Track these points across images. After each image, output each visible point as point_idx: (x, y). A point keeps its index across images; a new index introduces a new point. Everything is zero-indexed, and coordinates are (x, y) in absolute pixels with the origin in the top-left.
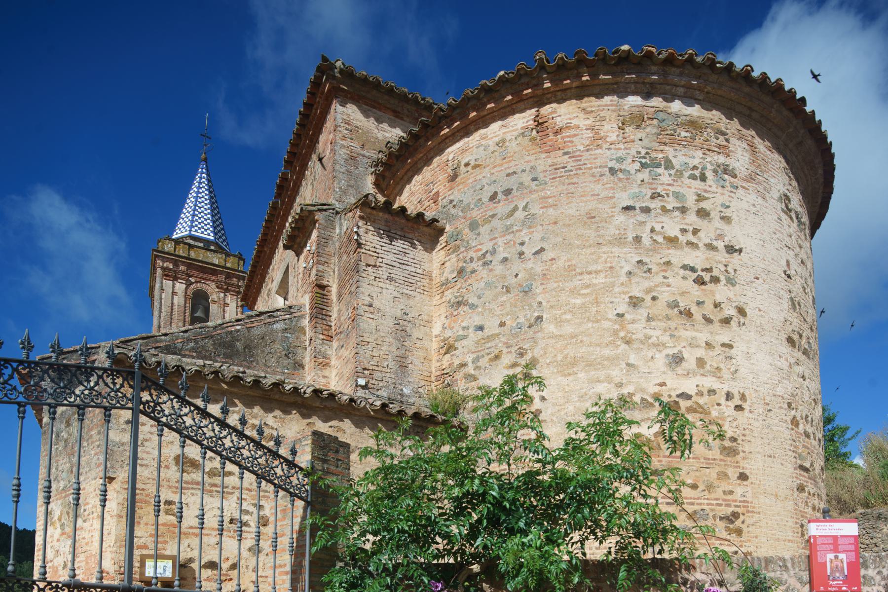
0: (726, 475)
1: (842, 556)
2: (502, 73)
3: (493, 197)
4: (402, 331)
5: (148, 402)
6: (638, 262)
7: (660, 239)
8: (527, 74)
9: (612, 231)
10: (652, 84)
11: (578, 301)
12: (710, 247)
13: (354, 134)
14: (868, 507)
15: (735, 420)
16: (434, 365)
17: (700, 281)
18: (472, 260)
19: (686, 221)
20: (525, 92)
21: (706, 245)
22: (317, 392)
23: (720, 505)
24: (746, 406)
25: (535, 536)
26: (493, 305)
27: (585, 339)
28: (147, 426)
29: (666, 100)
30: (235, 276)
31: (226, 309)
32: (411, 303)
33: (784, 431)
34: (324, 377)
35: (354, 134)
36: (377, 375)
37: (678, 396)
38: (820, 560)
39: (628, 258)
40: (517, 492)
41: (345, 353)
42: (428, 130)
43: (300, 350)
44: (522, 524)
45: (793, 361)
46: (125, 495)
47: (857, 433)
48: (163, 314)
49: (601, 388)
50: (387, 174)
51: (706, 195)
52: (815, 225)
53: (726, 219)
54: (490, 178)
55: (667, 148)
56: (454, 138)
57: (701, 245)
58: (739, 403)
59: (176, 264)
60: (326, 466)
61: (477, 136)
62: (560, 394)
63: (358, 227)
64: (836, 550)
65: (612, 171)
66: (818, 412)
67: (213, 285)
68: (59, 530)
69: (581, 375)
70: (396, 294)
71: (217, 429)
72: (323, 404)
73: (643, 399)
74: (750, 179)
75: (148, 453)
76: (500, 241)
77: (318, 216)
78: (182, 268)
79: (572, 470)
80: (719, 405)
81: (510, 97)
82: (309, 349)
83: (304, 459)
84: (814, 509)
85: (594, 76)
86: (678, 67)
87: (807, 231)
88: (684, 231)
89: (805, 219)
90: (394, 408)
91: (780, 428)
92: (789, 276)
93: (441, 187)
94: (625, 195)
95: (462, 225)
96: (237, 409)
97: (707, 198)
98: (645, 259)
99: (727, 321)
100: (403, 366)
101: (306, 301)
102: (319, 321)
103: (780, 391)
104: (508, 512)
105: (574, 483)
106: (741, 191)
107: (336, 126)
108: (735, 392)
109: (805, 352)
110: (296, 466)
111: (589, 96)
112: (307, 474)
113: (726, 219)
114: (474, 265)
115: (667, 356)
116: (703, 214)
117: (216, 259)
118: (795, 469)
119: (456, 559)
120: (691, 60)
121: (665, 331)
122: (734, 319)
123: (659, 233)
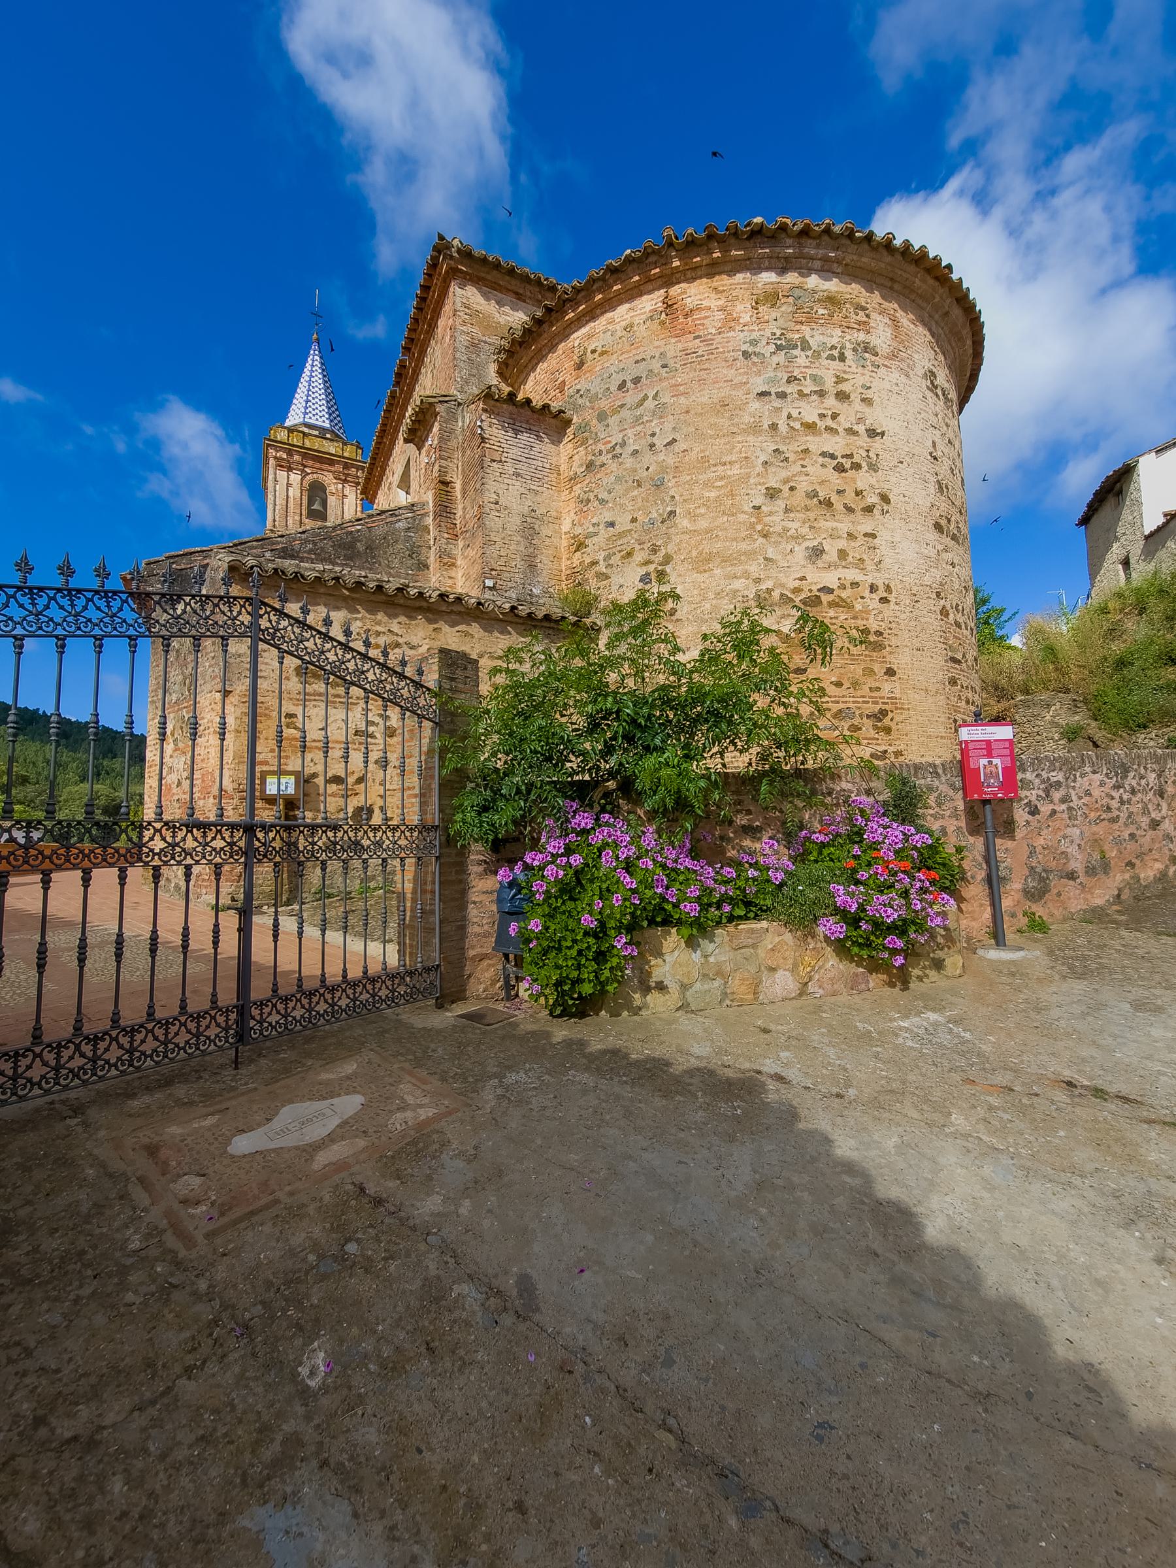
0: (872, 671)
1: (997, 761)
2: (628, 251)
3: (622, 386)
4: (529, 531)
5: (267, 629)
6: (775, 451)
7: (797, 425)
8: (654, 252)
9: (747, 419)
10: (787, 258)
11: (713, 494)
12: (851, 432)
13: (475, 318)
14: (1028, 693)
15: (880, 612)
16: (565, 563)
17: (840, 469)
18: (601, 452)
19: (825, 405)
20: (653, 272)
21: (846, 430)
22: (442, 596)
23: (868, 702)
24: (891, 598)
25: (674, 752)
26: (624, 501)
27: (720, 533)
28: (269, 656)
29: (802, 275)
30: (353, 466)
31: (345, 505)
32: (539, 499)
33: (933, 622)
34: (450, 578)
35: (475, 318)
36: (505, 575)
37: (819, 590)
38: (972, 766)
39: (763, 446)
40: (653, 706)
41: (471, 552)
42: (554, 311)
43: (424, 550)
44: (658, 742)
45: (940, 547)
46: (245, 708)
47: (1014, 615)
48: (277, 507)
49: (738, 584)
50: (510, 362)
51: (846, 376)
52: (963, 400)
53: (867, 401)
54: (617, 366)
55: (803, 328)
56: (579, 322)
57: (840, 430)
58: (885, 595)
59: (290, 453)
60: (454, 684)
61: (602, 320)
62: (695, 592)
63: (482, 421)
64: (989, 755)
65: (746, 355)
66: (970, 599)
67: (331, 476)
68: (172, 745)
69: (717, 571)
70: (523, 490)
71: (340, 652)
72: (449, 608)
73: (782, 595)
74: (893, 356)
75: (266, 664)
76: (630, 433)
77: (440, 408)
78: (297, 458)
79: (709, 682)
80: (862, 598)
81: (637, 278)
82: (433, 549)
83: (431, 678)
84: (968, 702)
85: (725, 251)
86: (814, 238)
87: (955, 408)
88: (822, 416)
89: (953, 395)
90: (523, 610)
91: (928, 620)
92: (935, 458)
93: (567, 376)
94: (759, 380)
95: (589, 416)
96: (359, 616)
97: (847, 380)
98: (782, 448)
99: (869, 509)
100: (531, 565)
101: (429, 497)
102: (444, 519)
103: (927, 580)
104: (643, 729)
105: (710, 697)
106: (883, 370)
107: (456, 311)
108: (880, 583)
109: (954, 538)
110: (422, 686)
111: (720, 273)
112: (436, 695)
113: (867, 401)
114: (603, 459)
115: (807, 548)
116: (842, 396)
117: (332, 448)
118: (946, 661)
119: (590, 776)
120: (827, 231)
121: (804, 523)
122: (877, 506)
123: (797, 419)
